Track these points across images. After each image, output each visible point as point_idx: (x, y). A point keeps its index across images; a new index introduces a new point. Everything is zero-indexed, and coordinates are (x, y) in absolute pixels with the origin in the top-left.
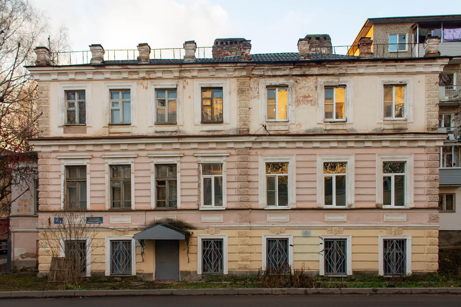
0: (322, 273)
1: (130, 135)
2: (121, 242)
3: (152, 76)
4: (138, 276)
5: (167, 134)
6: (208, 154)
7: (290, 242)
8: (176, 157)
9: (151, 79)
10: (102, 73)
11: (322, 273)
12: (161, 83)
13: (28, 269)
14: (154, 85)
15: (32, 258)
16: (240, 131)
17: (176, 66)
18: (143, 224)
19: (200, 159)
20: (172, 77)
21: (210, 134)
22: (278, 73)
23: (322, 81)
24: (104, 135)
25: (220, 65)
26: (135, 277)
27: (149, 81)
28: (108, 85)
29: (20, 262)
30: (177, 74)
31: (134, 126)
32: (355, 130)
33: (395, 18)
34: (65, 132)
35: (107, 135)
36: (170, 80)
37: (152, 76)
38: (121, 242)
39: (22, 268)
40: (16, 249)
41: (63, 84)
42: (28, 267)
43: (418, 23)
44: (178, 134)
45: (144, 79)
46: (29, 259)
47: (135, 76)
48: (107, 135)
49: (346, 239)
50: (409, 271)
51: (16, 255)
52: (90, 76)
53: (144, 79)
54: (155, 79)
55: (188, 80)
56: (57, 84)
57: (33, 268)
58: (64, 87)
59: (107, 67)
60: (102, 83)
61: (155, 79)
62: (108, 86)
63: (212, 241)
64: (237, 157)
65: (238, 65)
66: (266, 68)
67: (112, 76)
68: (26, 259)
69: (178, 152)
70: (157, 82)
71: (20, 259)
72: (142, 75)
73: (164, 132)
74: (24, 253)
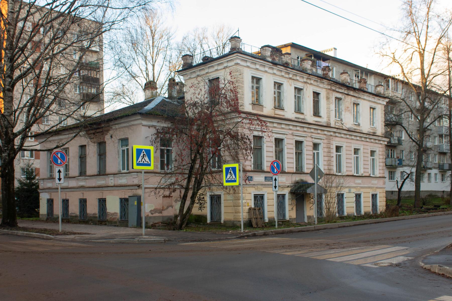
0: (355, 214)
1: (284, 117)
2: (281, 196)
3: (295, 78)
4: (291, 220)
5: (300, 120)
6: (282, 132)
7: (345, 196)
8: (304, 137)
9: (293, 79)
10: (273, 69)
11: (355, 214)
12: (297, 84)
13: (156, 225)
14: (295, 84)
15: (159, 213)
16: (328, 124)
17: (306, 75)
18: (291, 183)
19: (313, 139)
20: (302, 81)
21: (317, 123)
22: (340, 91)
23: (353, 99)
24: (272, 115)
25: (324, 80)
26: (288, 221)
27: (292, 81)
28: (274, 78)
29: (150, 217)
30: (305, 80)
31: (286, 111)
32: (362, 130)
33: (303, 46)
34: (253, 109)
35: (273, 115)
36: (279, 77)
37: (295, 78)
38: (281, 196)
39: (151, 223)
40: (146, 205)
41: (251, 71)
42: (156, 222)
43: (313, 54)
44: (304, 121)
45: (290, 78)
46: (157, 214)
47: (287, 76)
48: (273, 116)
49: (361, 194)
50: (346, 214)
51: (146, 211)
52: (267, 69)
53: (290, 78)
54: (295, 80)
55: (308, 85)
56: (249, 69)
57: (160, 224)
58: (252, 73)
59: (278, 66)
60: (271, 75)
61: (295, 80)
62: (274, 79)
63: (215, 197)
64: (326, 140)
65: (330, 82)
66: (337, 86)
67: (260, 67)
68: (154, 215)
69: (304, 133)
70: (296, 82)
71: (150, 215)
72: (291, 76)
73: (299, 118)
74: (153, 209)
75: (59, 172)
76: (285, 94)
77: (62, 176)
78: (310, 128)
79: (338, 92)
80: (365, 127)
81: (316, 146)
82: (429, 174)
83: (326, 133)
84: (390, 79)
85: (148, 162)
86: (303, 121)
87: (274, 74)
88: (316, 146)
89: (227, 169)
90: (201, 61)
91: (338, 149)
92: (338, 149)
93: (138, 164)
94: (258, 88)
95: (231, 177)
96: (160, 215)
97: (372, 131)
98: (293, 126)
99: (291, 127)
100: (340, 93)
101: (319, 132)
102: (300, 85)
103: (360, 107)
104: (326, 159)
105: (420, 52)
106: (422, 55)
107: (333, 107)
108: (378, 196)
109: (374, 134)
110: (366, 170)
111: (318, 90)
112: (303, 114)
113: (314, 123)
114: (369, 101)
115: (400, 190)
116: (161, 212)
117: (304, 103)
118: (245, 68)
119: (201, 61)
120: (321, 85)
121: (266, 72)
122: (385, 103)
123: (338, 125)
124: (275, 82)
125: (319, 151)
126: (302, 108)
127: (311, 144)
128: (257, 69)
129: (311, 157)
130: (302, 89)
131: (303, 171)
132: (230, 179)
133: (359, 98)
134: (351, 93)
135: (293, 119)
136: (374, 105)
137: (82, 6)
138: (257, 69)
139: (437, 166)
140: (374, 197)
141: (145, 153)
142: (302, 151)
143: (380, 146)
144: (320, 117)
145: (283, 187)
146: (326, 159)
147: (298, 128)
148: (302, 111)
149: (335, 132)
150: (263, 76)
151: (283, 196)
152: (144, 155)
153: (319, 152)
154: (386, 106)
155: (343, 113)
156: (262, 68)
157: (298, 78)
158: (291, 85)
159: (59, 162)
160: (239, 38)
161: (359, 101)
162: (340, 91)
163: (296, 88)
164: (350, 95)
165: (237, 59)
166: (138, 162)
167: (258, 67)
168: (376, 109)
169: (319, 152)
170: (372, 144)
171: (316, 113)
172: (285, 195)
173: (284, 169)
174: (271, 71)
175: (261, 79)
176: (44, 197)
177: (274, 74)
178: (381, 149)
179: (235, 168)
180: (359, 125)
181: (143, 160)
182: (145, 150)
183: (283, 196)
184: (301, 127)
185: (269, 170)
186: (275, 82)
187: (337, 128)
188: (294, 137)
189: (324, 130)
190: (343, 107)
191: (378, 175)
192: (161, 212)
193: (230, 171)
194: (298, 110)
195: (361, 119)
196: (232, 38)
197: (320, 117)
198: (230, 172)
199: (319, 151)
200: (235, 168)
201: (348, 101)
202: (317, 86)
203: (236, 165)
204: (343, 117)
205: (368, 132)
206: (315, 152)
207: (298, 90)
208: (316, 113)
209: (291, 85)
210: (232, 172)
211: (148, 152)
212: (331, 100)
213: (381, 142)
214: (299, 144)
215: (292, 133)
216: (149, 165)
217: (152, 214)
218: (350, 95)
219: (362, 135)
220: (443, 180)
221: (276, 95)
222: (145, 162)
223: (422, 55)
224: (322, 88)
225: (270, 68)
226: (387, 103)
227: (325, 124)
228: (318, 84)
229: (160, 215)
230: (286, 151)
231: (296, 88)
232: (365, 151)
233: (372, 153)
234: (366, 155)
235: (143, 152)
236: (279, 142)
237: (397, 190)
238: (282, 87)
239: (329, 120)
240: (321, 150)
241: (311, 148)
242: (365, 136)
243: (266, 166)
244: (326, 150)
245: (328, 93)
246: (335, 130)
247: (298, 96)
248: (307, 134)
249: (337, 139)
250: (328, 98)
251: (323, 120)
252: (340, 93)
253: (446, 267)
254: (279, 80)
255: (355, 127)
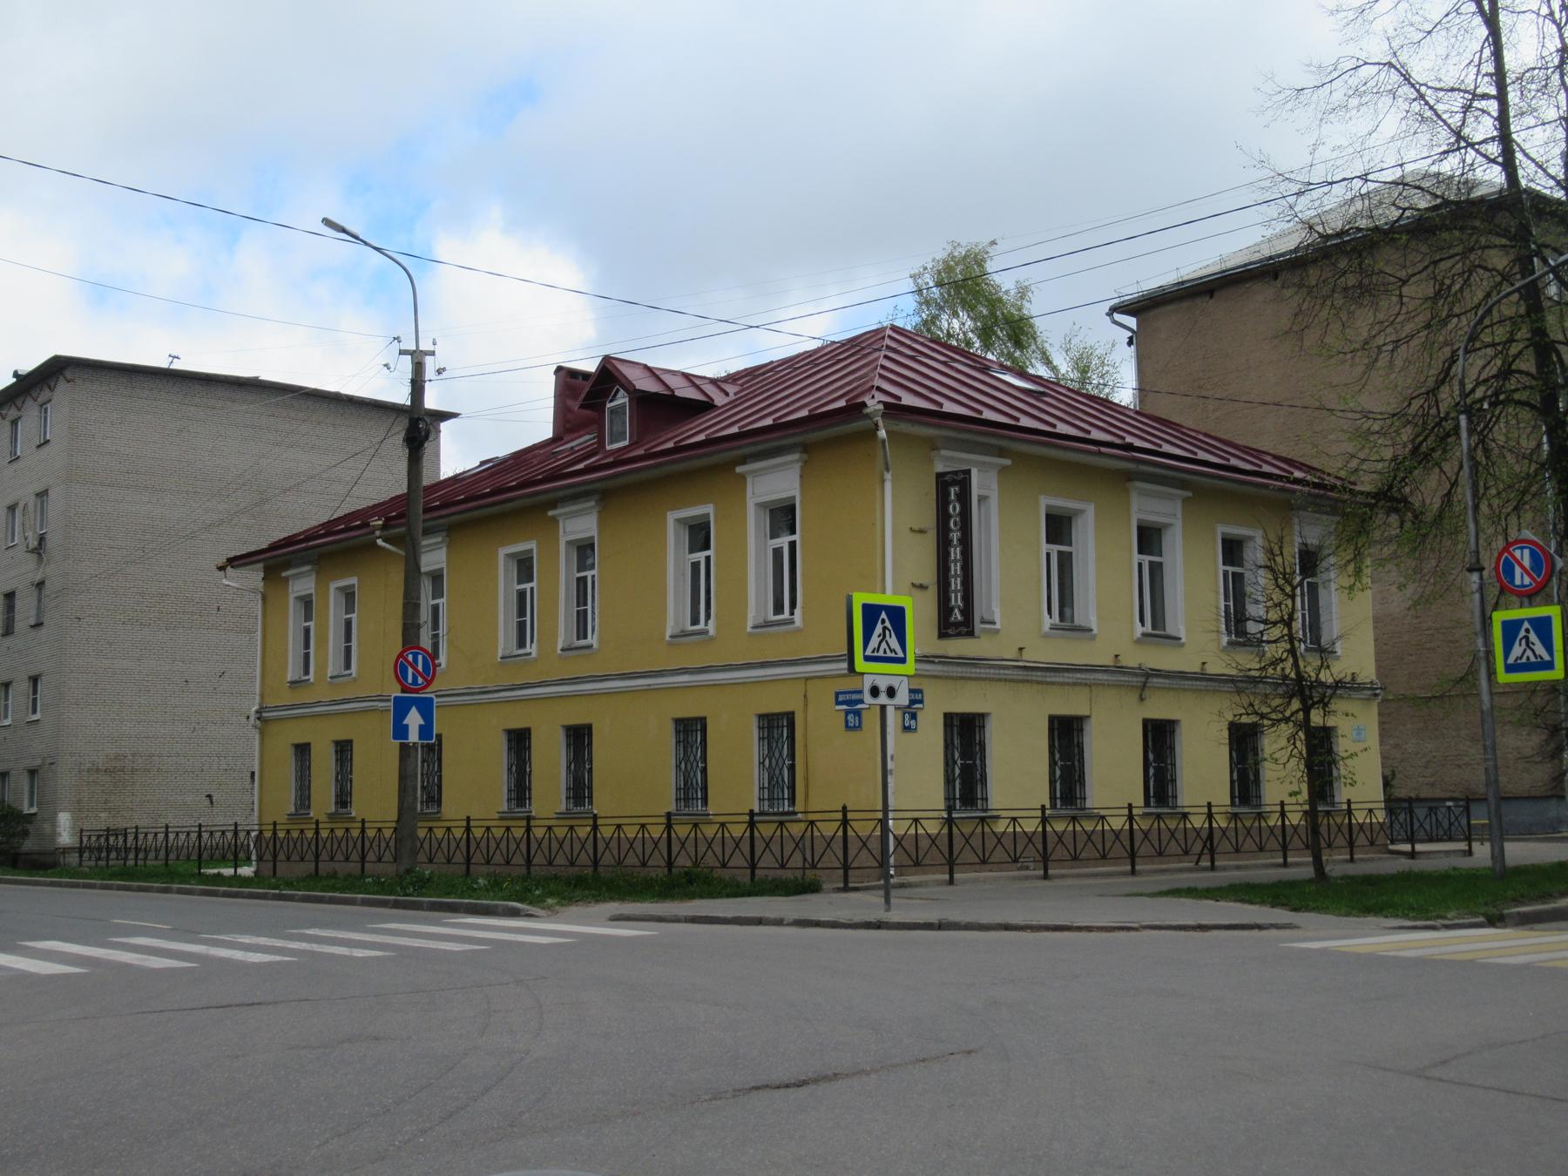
85: (1541, 658)
89: (1511, 629)
93: (1510, 669)
95: (1529, 652)
125: (1070, 544)
132: (881, 653)
137: (1356, 420)
141: (888, 624)
152: (885, 628)
153: (1161, 564)
166: (866, 654)
169: (1161, 564)
181: (884, 645)
182: (1530, 621)
193: (1522, 633)
198: (1527, 638)
199: (1070, 544)
210: (1533, 637)
216: (1549, 666)
222: (888, 650)
235: (883, 621)
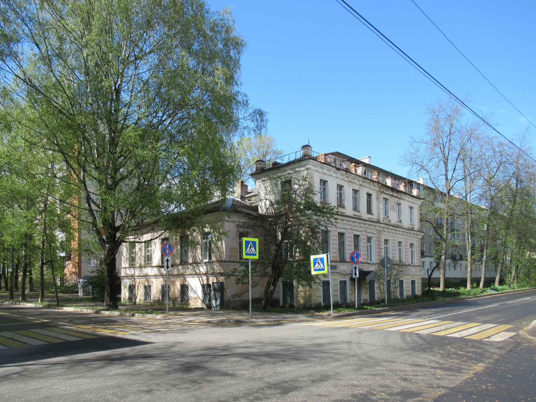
3: (353, 181)
5: (357, 217)
22: (387, 192)
30: (361, 183)
32: (403, 226)
40: (228, 290)
45: (350, 182)
46: (237, 298)
47: (347, 179)
53: (350, 182)
55: (363, 187)
58: (320, 177)
59: (341, 171)
70: (354, 185)
71: (231, 299)
72: (350, 179)
74: (233, 294)
75: (167, 261)
76: (345, 195)
77: (170, 265)
78: (365, 224)
79: (385, 193)
80: (406, 223)
81: (369, 239)
82: (461, 264)
83: (377, 228)
84: (414, 184)
86: (359, 217)
87: (337, 177)
88: (369, 239)
90: (271, 166)
91: (386, 241)
92: (386, 241)
93: (247, 254)
94: (324, 189)
95: (319, 266)
96: (239, 299)
97: (411, 227)
98: (352, 221)
99: (351, 223)
100: (387, 194)
101: (372, 227)
102: (356, 187)
103: (402, 206)
104: (377, 250)
105: (444, 162)
106: (446, 164)
107: (382, 206)
108: (416, 282)
109: (412, 229)
110: (407, 260)
111: (370, 192)
112: (359, 211)
113: (368, 219)
114: (409, 201)
115: (430, 276)
116: (240, 297)
117: (360, 202)
118: (315, 172)
119: (271, 166)
120: (373, 188)
121: (331, 175)
122: (420, 203)
123: (386, 221)
124: (337, 184)
126: (358, 207)
127: (366, 238)
128: (324, 173)
129: (366, 249)
130: (358, 191)
131: (345, 260)
132: (318, 268)
133: (401, 199)
134: (395, 194)
135: (352, 216)
136: (412, 205)
138: (324, 173)
139: (450, 257)
140: (413, 282)
141: (252, 244)
142: (358, 243)
143: (417, 239)
144: (372, 214)
145: (344, 275)
146: (377, 250)
147: (356, 224)
148: (358, 209)
149: (384, 228)
150: (328, 179)
151: (345, 282)
152: (251, 246)
154: (420, 206)
155: (389, 211)
156: (328, 173)
157: (355, 181)
158: (350, 187)
159: (167, 253)
160: (310, 146)
161: (401, 201)
162: (387, 192)
163: (353, 190)
164: (394, 196)
165: (311, 164)
167: (325, 171)
168: (414, 208)
170: (411, 238)
171: (369, 211)
172: (346, 281)
173: (345, 258)
174: (334, 175)
175: (327, 181)
176: (125, 284)
177: (337, 177)
178: (418, 242)
179: (323, 258)
180: (401, 221)
181: (250, 250)
182: (252, 242)
183: (345, 282)
184: (358, 223)
185: (350, 261)
186: (337, 184)
187: (386, 224)
188: (353, 231)
189: (375, 226)
190: (389, 206)
191: (416, 264)
192: (240, 297)
194: (355, 208)
195: (402, 216)
196: (303, 147)
197: (372, 214)
198: (319, 262)
200: (323, 258)
201: (392, 201)
202: (370, 188)
203: (324, 256)
204: (389, 215)
205: (408, 227)
206: (369, 244)
207: (355, 192)
208: (369, 211)
209: (350, 187)
210: (320, 262)
211: (254, 243)
212: (380, 200)
213: (418, 236)
214: (357, 237)
215: (352, 228)
216: (255, 255)
217: (233, 298)
218: (394, 196)
219: (404, 230)
220: (455, 268)
221: (338, 196)
223: (446, 164)
224: (373, 190)
225: (334, 172)
226: (422, 203)
227: (375, 221)
228: (371, 186)
229: (239, 299)
230: (347, 243)
231: (353, 190)
232: (406, 243)
233: (412, 245)
234: (407, 247)
236: (341, 235)
237: (428, 277)
238: (342, 189)
239: (379, 217)
240: (373, 243)
241: (365, 241)
242: (406, 231)
243: (347, 257)
244: (377, 243)
245: (378, 194)
246: (384, 226)
247: (355, 197)
248: (363, 229)
249: (385, 233)
250: (378, 199)
251: (374, 217)
252: (387, 194)
253: (89, 311)
254: (341, 183)
255: (398, 224)
